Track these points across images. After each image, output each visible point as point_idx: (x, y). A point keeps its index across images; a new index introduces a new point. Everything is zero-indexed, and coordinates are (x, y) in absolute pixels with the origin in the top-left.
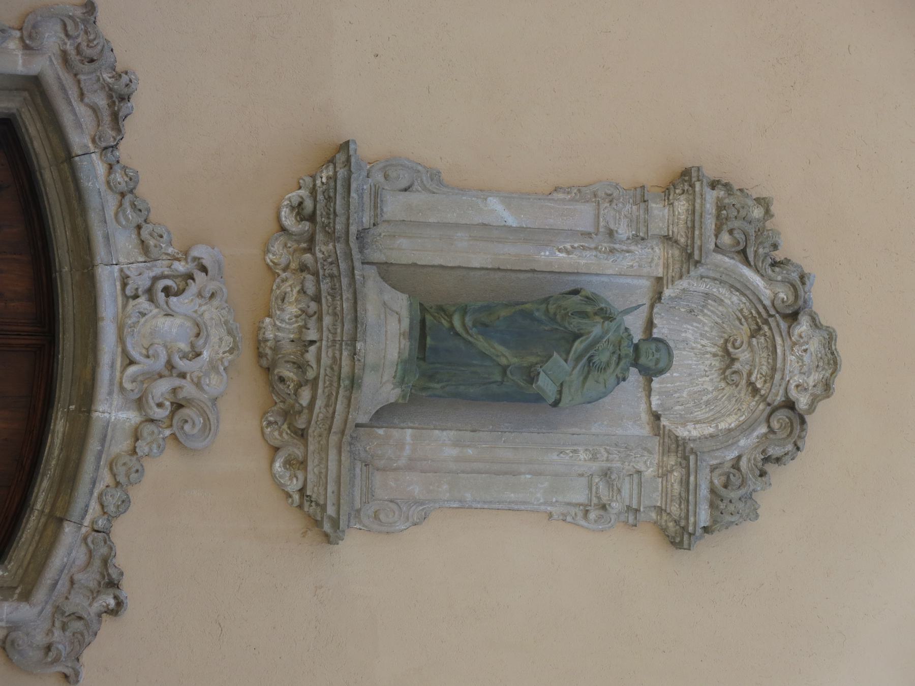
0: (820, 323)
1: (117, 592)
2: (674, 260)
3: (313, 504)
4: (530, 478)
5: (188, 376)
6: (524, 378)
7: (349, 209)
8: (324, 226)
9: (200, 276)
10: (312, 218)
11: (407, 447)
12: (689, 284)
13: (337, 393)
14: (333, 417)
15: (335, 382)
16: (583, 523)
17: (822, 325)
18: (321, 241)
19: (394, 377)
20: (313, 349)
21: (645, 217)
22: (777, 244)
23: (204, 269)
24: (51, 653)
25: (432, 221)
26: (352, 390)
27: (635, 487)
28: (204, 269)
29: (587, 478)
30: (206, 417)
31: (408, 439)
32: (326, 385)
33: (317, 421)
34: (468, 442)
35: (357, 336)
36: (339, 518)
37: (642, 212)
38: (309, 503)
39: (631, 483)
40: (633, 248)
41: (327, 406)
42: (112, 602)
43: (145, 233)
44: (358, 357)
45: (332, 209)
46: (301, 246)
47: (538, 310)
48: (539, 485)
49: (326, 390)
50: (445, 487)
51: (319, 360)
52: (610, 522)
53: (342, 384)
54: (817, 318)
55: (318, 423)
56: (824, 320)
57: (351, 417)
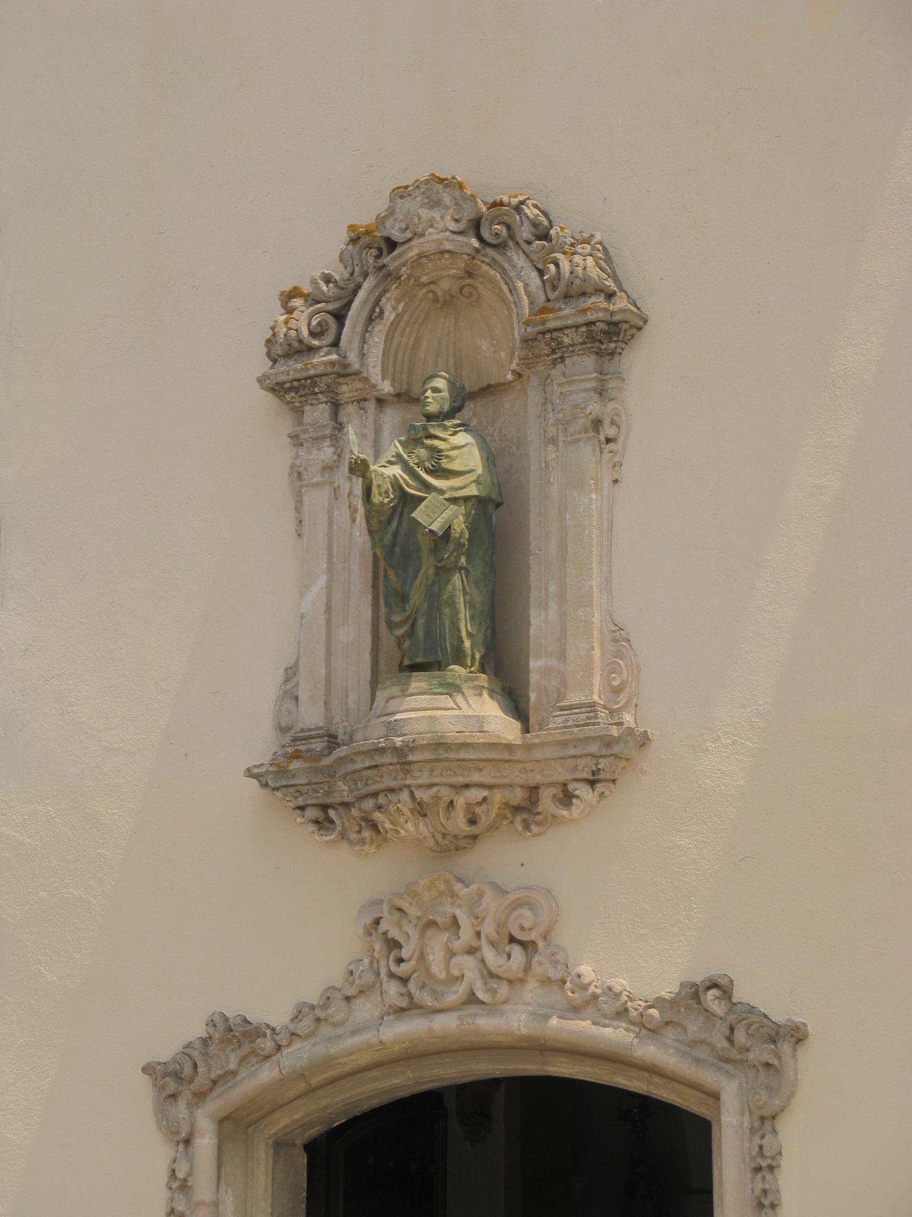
1: (701, 989)
2: (631, 327)
3: (600, 767)
5: (478, 929)
9: (383, 927)
12: (375, 367)
16: (620, 441)
17: (389, 207)
19: (451, 695)
23: (377, 922)
24: (770, 1060)
25: (324, 671)
28: (377, 922)
32: (452, 774)
34: (541, 592)
36: (600, 737)
37: (307, 436)
42: (713, 992)
43: (350, 992)
48: (576, 502)
49: (458, 772)
56: (383, 204)
57: (481, 740)
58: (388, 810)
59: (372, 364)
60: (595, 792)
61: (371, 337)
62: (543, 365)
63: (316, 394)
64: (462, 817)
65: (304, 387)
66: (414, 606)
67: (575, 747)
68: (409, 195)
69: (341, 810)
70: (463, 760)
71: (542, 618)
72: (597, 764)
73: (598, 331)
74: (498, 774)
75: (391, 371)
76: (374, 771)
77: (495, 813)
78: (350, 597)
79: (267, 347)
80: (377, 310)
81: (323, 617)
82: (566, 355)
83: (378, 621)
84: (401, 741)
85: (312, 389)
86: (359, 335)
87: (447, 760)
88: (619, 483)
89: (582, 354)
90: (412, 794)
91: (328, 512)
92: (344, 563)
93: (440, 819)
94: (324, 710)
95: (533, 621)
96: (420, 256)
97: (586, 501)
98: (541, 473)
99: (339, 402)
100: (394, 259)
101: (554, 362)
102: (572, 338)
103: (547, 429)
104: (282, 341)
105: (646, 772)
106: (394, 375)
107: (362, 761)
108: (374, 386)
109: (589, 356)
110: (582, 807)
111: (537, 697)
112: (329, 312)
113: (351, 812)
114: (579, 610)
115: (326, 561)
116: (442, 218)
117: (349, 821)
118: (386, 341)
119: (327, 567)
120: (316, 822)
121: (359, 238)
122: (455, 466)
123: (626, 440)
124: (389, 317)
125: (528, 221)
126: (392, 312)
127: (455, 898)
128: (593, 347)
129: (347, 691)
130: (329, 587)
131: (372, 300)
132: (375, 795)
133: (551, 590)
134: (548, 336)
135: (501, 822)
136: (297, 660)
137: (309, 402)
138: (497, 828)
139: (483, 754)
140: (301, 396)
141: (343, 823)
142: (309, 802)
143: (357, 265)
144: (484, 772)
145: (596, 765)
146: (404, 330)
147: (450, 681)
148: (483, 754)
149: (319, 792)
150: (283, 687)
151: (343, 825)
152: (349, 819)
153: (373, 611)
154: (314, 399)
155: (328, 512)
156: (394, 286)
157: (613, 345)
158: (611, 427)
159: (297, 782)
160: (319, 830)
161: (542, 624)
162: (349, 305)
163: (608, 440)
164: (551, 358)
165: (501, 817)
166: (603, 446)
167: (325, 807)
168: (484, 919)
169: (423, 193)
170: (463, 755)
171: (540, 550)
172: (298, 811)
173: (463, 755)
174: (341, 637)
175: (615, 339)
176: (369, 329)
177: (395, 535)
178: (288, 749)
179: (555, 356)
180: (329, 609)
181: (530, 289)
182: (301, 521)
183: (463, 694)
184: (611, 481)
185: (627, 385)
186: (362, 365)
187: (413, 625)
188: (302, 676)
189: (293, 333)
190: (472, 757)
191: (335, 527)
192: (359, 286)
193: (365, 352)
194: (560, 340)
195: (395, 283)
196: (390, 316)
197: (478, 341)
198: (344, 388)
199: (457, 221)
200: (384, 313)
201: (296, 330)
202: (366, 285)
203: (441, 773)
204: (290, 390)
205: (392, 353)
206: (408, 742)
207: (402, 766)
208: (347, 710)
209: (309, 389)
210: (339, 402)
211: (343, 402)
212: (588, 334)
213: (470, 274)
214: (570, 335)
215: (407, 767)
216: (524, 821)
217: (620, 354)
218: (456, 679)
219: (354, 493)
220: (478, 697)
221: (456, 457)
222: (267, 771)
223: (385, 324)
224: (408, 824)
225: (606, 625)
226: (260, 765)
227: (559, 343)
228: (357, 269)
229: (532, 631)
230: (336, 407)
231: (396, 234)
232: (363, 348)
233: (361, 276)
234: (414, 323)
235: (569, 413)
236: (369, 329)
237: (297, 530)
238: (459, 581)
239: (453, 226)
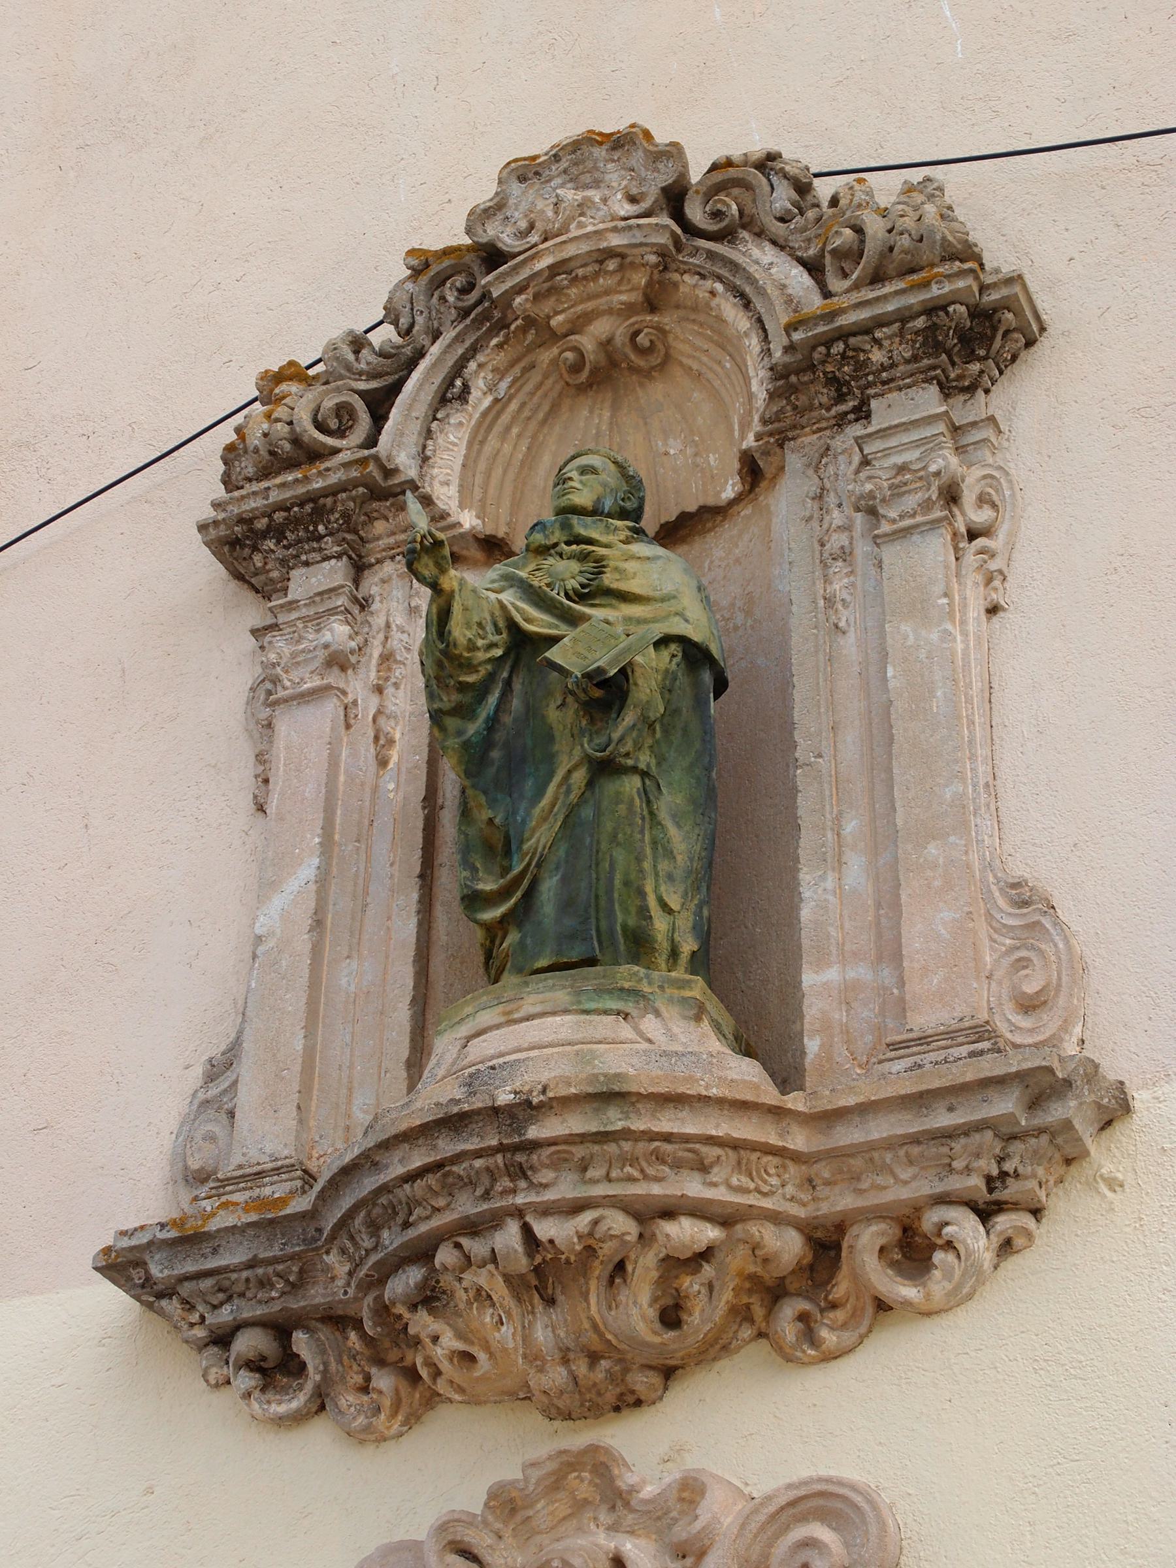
0: (491, 200)
3: (1008, 1166)
4: (894, 666)
6: (614, 716)
7: (235, 1226)
8: (294, 1288)
10: (281, 1329)
11: (851, 974)
13: (652, 1137)
14: (735, 1145)
15: (619, 1146)
17: (497, 194)
18: (326, 1288)
19: (626, 1016)
20: (544, 1229)
21: (305, 605)
22: (350, 338)
26: (629, 1093)
27: (893, 442)
29: (883, 548)
30: (792, 1511)
31: (832, 974)
32: (636, 1174)
33: (760, 1192)
35: (480, 1109)
36: (1020, 1077)
38: (1010, 1181)
39: (887, 452)
40: (379, 621)
41: (703, 1168)
44: (535, 1094)
45: (245, 1274)
46: (357, 1346)
47: (460, 733)
49: (650, 1171)
50: (932, 850)
51: (576, 1208)
52: (992, 477)
53: (619, 1125)
54: (482, 207)
55: (766, 1189)
57: (714, 1091)
58: (452, 1304)
59: (441, 478)
60: (992, 1236)
61: (441, 431)
62: (814, 432)
63: (320, 538)
64: (645, 1306)
65: (296, 522)
66: (534, 854)
67: (951, 1109)
68: (537, 173)
69: (325, 1333)
70: (668, 1138)
71: (830, 883)
72: (1003, 1159)
73: (950, 328)
74: (745, 1181)
75: (478, 493)
76: (432, 1180)
77: (727, 1302)
78: (366, 905)
79: (225, 464)
80: (458, 383)
81: (306, 936)
82: (871, 391)
83: (428, 948)
84: (511, 1092)
85: (311, 528)
86: (419, 422)
87: (626, 1134)
88: (1001, 614)
89: (909, 386)
90: (527, 1230)
91: (330, 743)
92: (358, 841)
93: (589, 1308)
94: (295, 1122)
95: (806, 894)
96: (554, 270)
97: (934, 636)
98: (815, 616)
99: (364, 560)
100: (501, 279)
101: (841, 422)
102: (891, 351)
103: (826, 538)
104: (256, 442)
105: (1122, 1186)
106: (483, 501)
107: (400, 1161)
108: (444, 516)
109: (923, 389)
110: (958, 1273)
111: (822, 1046)
112: (362, 394)
113: (347, 1339)
114: (929, 846)
115: (319, 831)
116: (605, 200)
117: (340, 1361)
118: (470, 444)
119: (320, 843)
120: (255, 1365)
121: (427, 265)
122: (633, 586)
123: (1013, 534)
124: (480, 400)
125: (785, 182)
126: (485, 394)
127: (621, 1510)
128: (934, 368)
129: (350, 1089)
130: (323, 880)
131: (450, 362)
132: (423, 1253)
133: (848, 830)
134: (839, 347)
135: (736, 1332)
136: (240, 1033)
137: (304, 558)
138: (725, 1348)
139: (717, 1126)
140: (286, 547)
141: (326, 1364)
142: (246, 1315)
143: (422, 312)
144: (717, 1174)
145: (1000, 1160)
146: (508, 429)
147: (627, 985)
148: (717, 1126)
149: (272, 1286)
150: (200, 1094)
151: (325, 1372)
152: (340, 1356)
153: (420, 924)
154: (314, 550)
155: (330, 743)
156: (494, 342)
157: (975, 367)
158: (980, 507)
159: (223, 1263)
160: (263, 1390)
161: (830, 898)
162: (395, 389)
163: (972, 535)
164: (833, 412)
165: (741, 1314)
166: (961, 545)
167: (281, 1329)
168: (702, 1554)
169: (565, 171)
170: (667, 1123)
171: (820, 756)
172: (214, 1350)
173: (667, 1123)
174: (344, 981)
175: (982, 353)
176: (439, 416)
177: (493, 723)
178: (204, 1203)
179: (842, 408)
180: (318, 923)
181: (790, 291)
182: (266, 781)
183: (657, 1014)
184: (983, 612)
185: (1008, 440)
186: (421, 476)
187: (530, 893)
188: (247, 1071)
189: (281, 429)
190: (690, 1129)
191: (342, 778)
192: (420, 354)
193: (429, 453)
194: (862, 357)
195: (497, 335)
196: (480, 400)
197: (660, 443)
198: (380, 527)
199: (633, 200)
200: (469, 393)
201: (290, 423)
202: (435, 350)
203: (608, 1174)
204: (264, 534)
205: (482, 466)
206: (531, 1091)
207: (509, 1155)
208: (348, 1128)
209: (306, 530)
210: (364, 560)
211: (373, 560)
212: (926, 338)
213: (651, 305)
214: (886, 343)
215: (520, 1158)
216: (803, 1317)
217: (987, 391)
218: (641, 980)
219: (388, 712)
220: (693, 1023)
221: (635, 574)
222: (151, 1243)
223: (471, 416)
224: (504, 1329)
225: (995, 877)
226: (136, 1230)
227: (861, 366)
228: (420, 320)
229: (806, 913)
230: (359, 568)
231: (507, 240)
232: (424, 447)
233: (426, 333)
234: (529, 418)
235: (885, 484)
236: (439, 416)
237: (255, 797)
238: (640, 798)
239: (627, 209)
